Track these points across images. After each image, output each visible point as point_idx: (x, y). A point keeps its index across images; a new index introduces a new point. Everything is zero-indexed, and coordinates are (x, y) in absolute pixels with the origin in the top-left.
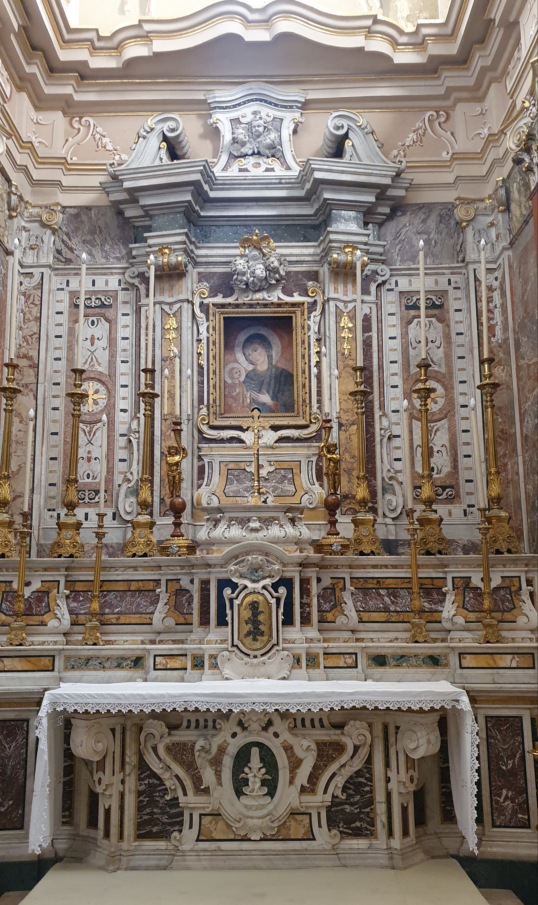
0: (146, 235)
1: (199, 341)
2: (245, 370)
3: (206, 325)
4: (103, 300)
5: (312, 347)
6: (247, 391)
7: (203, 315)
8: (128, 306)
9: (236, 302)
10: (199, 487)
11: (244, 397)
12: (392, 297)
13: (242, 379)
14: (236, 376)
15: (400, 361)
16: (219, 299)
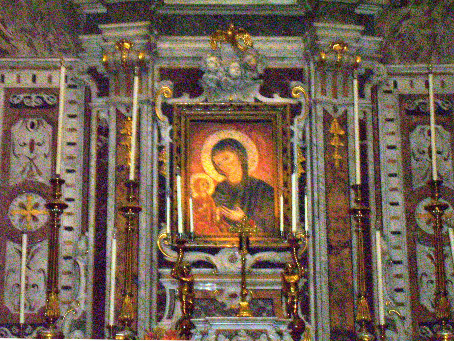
0: (101, 27)
1: (161, 148)
2: (215, 181)
3: (170, 128)
4: (46, 99)
5: (296, 156)
6: (217, 206)
7: (166, 119)
8: (76, 106)
9: (205, 104)
10: (159, 319)
11: (213, 215)
12: (390, 100)
13: (211, 191)
14: (202, 188)
15: (401, 174)
16: (185, 100)
